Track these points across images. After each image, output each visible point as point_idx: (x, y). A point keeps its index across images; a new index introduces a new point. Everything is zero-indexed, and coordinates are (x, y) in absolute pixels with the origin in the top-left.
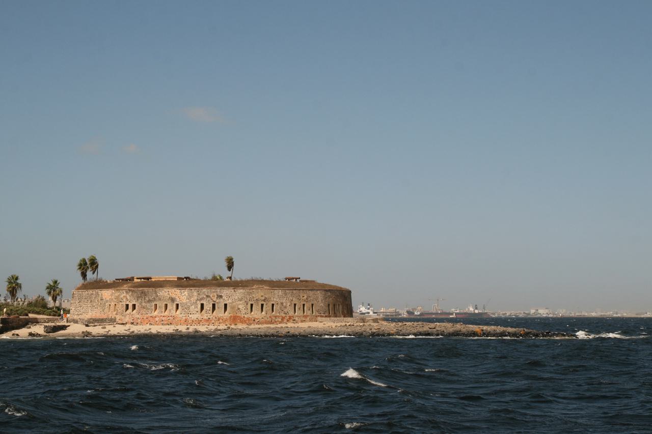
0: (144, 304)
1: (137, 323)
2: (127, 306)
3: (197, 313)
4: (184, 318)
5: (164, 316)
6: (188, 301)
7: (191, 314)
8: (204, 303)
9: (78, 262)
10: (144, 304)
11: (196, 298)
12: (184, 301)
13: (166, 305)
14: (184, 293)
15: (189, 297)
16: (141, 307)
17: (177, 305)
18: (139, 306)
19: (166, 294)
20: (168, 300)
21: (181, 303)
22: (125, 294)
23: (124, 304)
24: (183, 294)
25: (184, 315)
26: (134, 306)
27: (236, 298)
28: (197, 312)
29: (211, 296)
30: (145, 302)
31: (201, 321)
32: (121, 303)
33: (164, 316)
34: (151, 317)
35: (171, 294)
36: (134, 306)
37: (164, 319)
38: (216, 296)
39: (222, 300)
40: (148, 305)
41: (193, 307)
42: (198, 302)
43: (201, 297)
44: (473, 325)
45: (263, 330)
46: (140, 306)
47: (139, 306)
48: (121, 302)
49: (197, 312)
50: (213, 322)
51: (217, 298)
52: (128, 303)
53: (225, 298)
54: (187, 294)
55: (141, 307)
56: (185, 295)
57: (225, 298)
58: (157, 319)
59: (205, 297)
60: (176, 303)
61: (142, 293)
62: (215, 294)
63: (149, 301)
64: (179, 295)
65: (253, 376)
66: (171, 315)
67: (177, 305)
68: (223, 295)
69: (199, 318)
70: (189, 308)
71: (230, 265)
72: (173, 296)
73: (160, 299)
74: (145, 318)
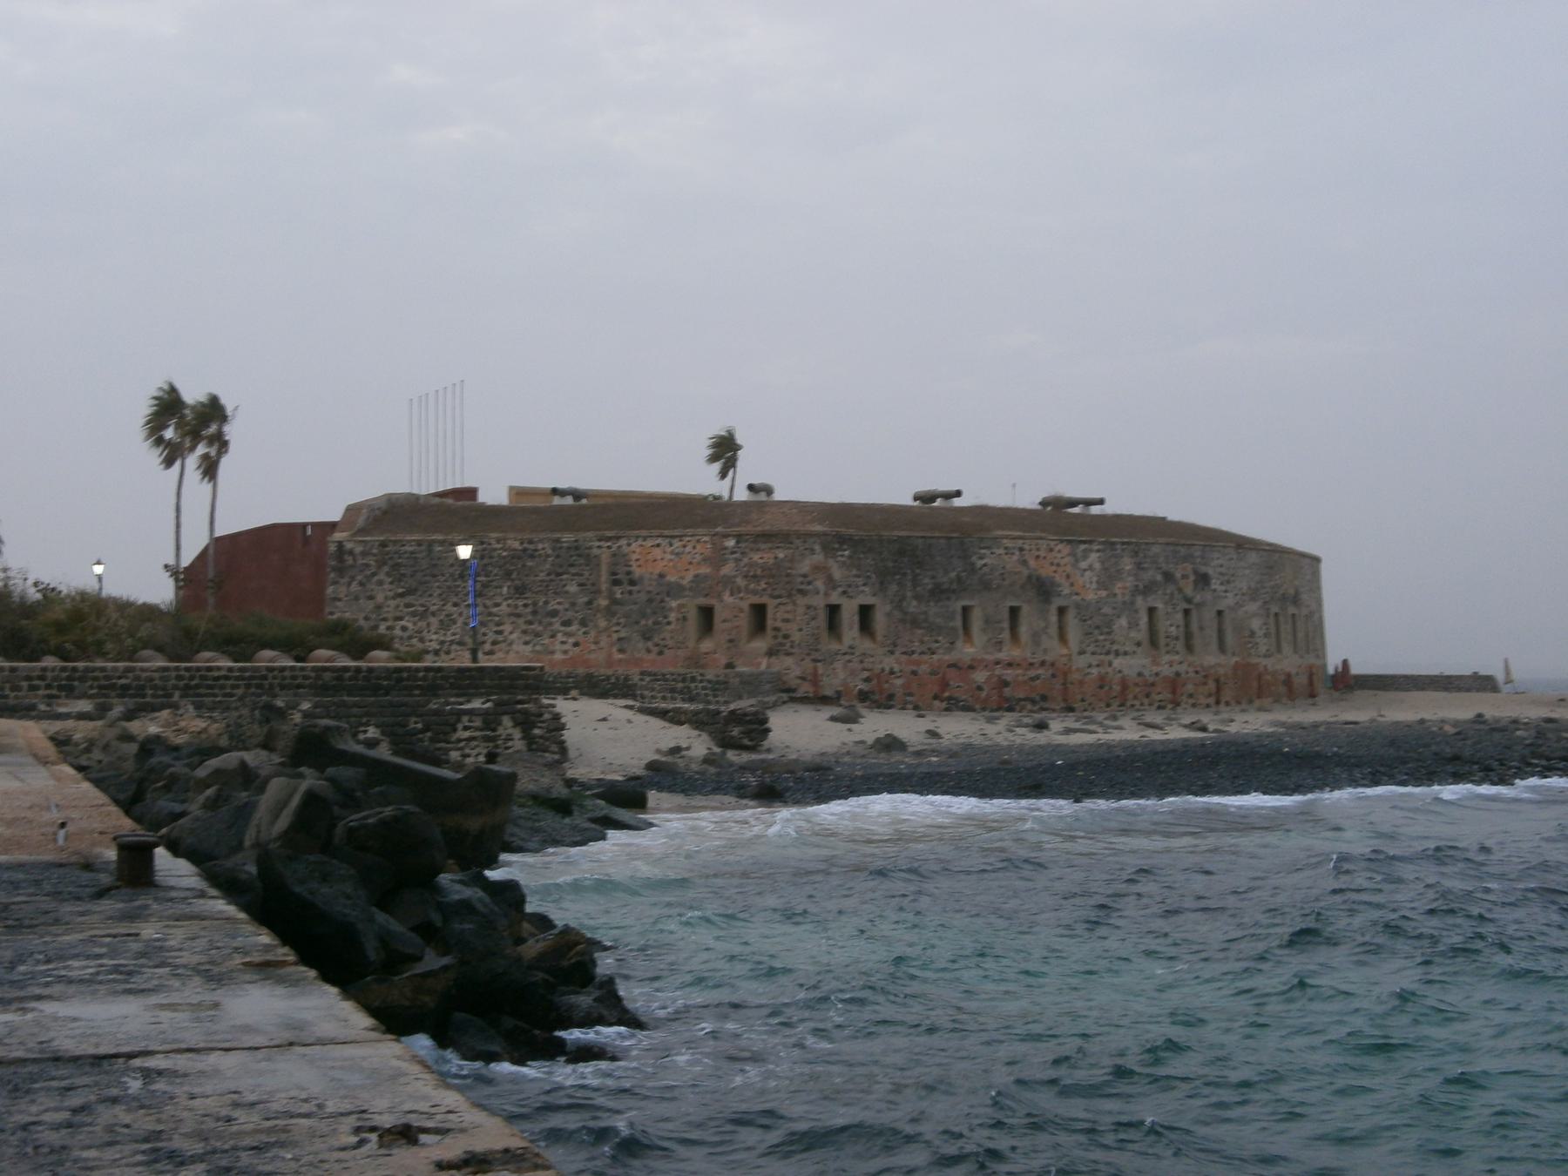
0: (913, 606)
1: (891, 697)
2: (833, 610)
3: (1139, 650)
4: (1095, 671)
5: (1010, 665)
6: (1103, 593)
7: (1117, 654)
8: (1160, 605)
9: (143, 409)
10: (913, 606)
11: (1129, 582)
12: (1091, 596)
13: (1014, 612)
14: (1085, 557)
15: (1108, 578)
16: (903, 621)
18: (889, 615)
19: (1012, 562)
20: (1022, 587)
21: (1078, 606)
22: (819, 558)
23: (819, 602)
24: (1083, 565)
25: (1094, 660)
26: (865, 612)
28: (1139, 644)
29: (1178, 575)
30: (917, 597)
31: (1153, 685)
32: (802, 601)
33: (1010, 665)
34: (952, 666)
35: (1032, 563)
36: (865, 612)
37: (1009, 674)
38: (1192, 578)
39: (1208, 596)
41: (1123, 622)
42: (1139, 600)
44: (1458, 778)
45: (1535, 713)
46: (898, 615)
47: (889, 615)
48: (800, 591)
49: (1139, 644)
50: (1190, 688)
51: (1196, 583)
52: (835, 598)
54: (1097, 566)
55: (903, 621)
56: (1091, 568)
58: (980, 676)
59: (1159, 578)
60: (1057, 602)
62: (1189, 567)
63: (938, 593)
64: (1069, 569)
65: (1275, 1121)
66: (1039, 658)
67: (1062, 611)
68: (1210, 571)
69: (1146, 673)
70: (1106, 627)
71: (725, 450)
72: (1046, 571)
73: (986, 586)
74: (924, 668)
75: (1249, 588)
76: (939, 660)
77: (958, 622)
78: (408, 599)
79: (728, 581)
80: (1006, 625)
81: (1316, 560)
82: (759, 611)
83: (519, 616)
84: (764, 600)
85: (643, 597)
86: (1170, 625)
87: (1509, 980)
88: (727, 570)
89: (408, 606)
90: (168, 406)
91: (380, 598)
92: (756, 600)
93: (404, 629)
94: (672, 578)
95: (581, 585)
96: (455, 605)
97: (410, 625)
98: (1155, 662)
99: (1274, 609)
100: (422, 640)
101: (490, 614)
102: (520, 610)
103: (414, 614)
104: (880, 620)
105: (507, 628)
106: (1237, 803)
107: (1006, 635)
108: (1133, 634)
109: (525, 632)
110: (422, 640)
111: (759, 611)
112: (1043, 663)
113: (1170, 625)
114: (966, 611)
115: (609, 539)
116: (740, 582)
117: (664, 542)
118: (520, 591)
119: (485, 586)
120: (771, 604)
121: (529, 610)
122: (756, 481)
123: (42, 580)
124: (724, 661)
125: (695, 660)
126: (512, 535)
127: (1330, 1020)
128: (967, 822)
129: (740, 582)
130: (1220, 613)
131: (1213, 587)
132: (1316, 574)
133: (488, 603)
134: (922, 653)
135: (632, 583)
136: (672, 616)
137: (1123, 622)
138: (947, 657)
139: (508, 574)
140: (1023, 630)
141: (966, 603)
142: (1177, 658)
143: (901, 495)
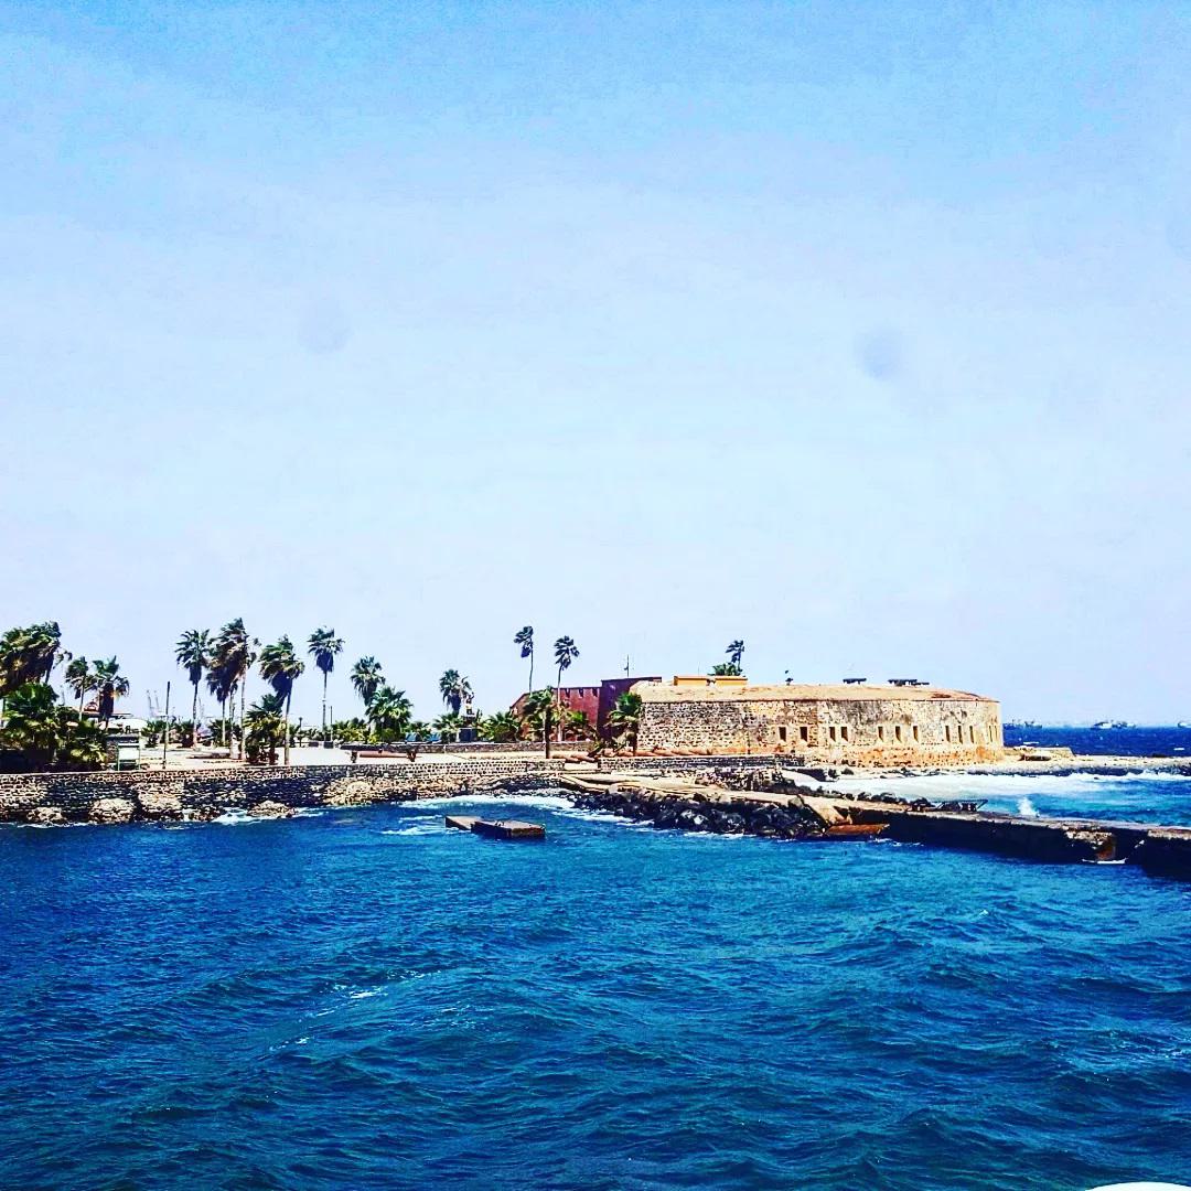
0: (860, 727)
2: (832, 729)
10: (860, 727)
13: (898, 729)
17: (915, 728)
23: (827, 726)
26: (844, 730)
27: (553, 698)
36: (844, 730)
37: (896, 753)
40: (868, 728)
43: (944, 714)
46: (855, 731)
52: (832, 725)
61: (856, 706)
63: (869, 721)
67: (915, 728)
72: (908, 713)
77: (877, 733)
78: (661, 725)
79: (791, 718)
80: (895, 733)
82: (804, 731)
84: (806, 725)
85: (757, 725)
86: (954, 732)
87: (1162, 884)
88: (791, 714)
91: (649, 725)
92: (802, 725)
94: (768, 717)
98: (949, 746)
99: (989, 724)
104: (849, 734)
105: (702, 737)
107: (895, 737)
111: (804, 731)
113: (954, 732)
114: (880, 729)
116: (796, 718)
118: (707, 722)
119: (693, 720)
120: (809, 727)
122: (1020, 719)
124: (791, 749)
125: (779, 748)
128: (318, 1094)
129: (796, 718)
130: (971, 727)
135: (752, 719)
136: (769, 732)
139: (701, 716)
140: (902, 737)
141: (880, 725)
143: (1061, 726)
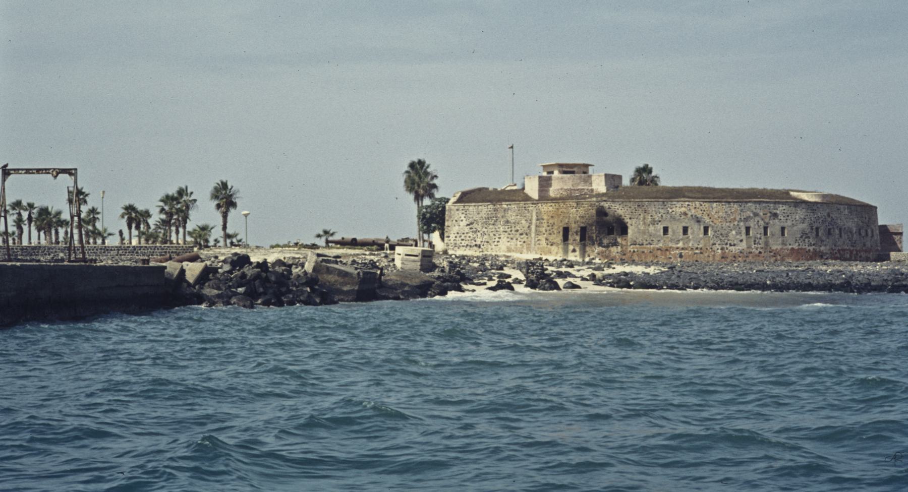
41: (734, 232)
53: (782, 218)
57: (782, 218)
59: (752, 215)
68: (778, 212)
75: (800, 218)
76: (653, 247)
78: (471, 226)
81: (876, 208)
83: (506, 232)
89: (471, 228)
90: (130, 209)
93: (470, 237)
95: (526, 220)
96: (486, 228)
97: (471, 236)
100: (475, 241)
101: (497, 231)
102: (507, 230)
103: (473, 232)
106: (357, 250)
108: (738, 237)
109: (508, 238)
110: (475, 241)
112: (697, 248)
115: (535, 204)
117: (554, 204)
121: (510, 229)
123: (904, 238)
126: (503, 203)
127: (765, 401)
131: (779, 218)
132: (876, 211)
133: (497, 227)
134: (647, 244)
137: (734, 232)
138: (657, 246)
142: (759, 246)
